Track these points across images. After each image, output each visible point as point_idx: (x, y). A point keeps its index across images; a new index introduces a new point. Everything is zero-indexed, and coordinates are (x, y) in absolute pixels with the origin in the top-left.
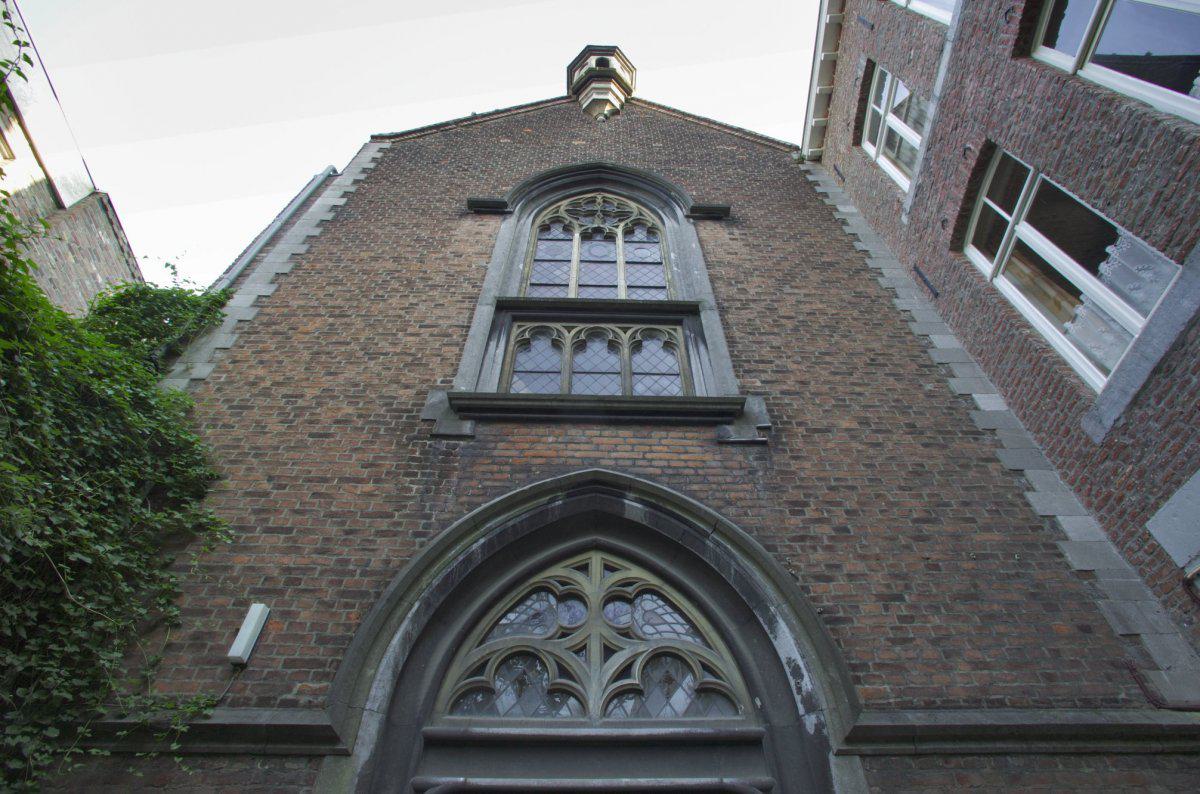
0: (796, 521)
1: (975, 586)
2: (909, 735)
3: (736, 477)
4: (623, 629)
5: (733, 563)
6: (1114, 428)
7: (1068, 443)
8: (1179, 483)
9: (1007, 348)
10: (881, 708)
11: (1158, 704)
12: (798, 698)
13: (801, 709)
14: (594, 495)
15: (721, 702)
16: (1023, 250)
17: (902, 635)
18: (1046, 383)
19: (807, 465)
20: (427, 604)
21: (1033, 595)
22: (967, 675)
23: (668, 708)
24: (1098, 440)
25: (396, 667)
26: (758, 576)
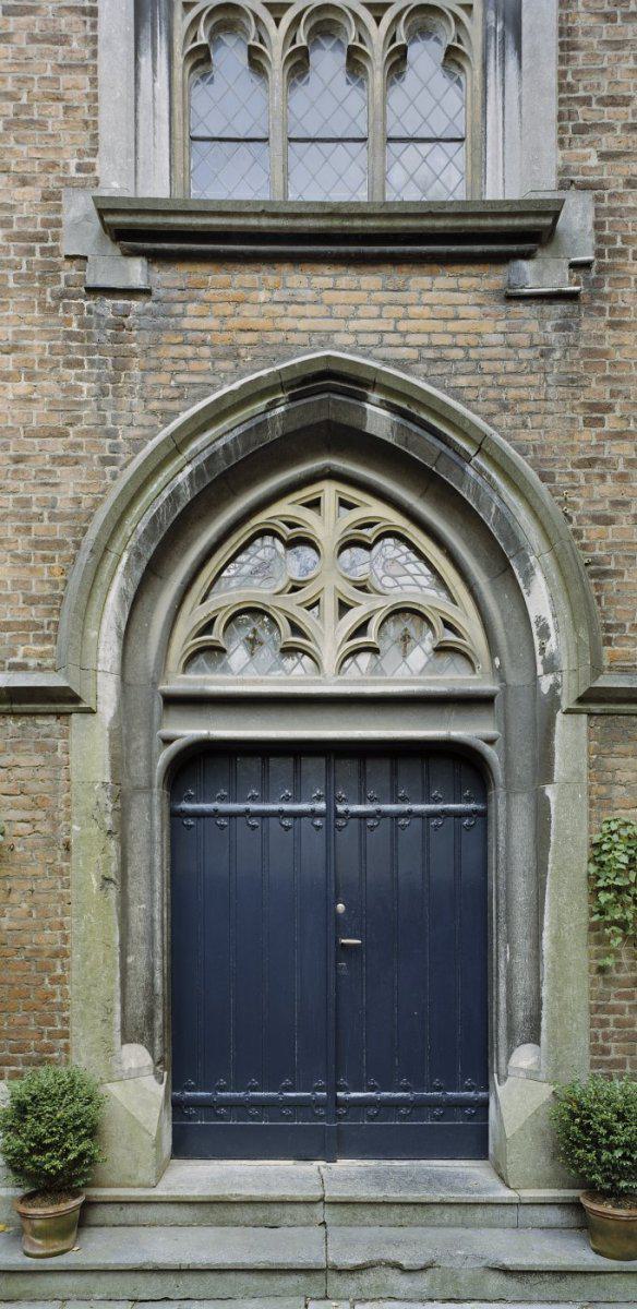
0: (591, 435)
5: (496, 498)
12: (539, 659)
13: (540, 670)
15: (459, 662)
26: (523, 517)
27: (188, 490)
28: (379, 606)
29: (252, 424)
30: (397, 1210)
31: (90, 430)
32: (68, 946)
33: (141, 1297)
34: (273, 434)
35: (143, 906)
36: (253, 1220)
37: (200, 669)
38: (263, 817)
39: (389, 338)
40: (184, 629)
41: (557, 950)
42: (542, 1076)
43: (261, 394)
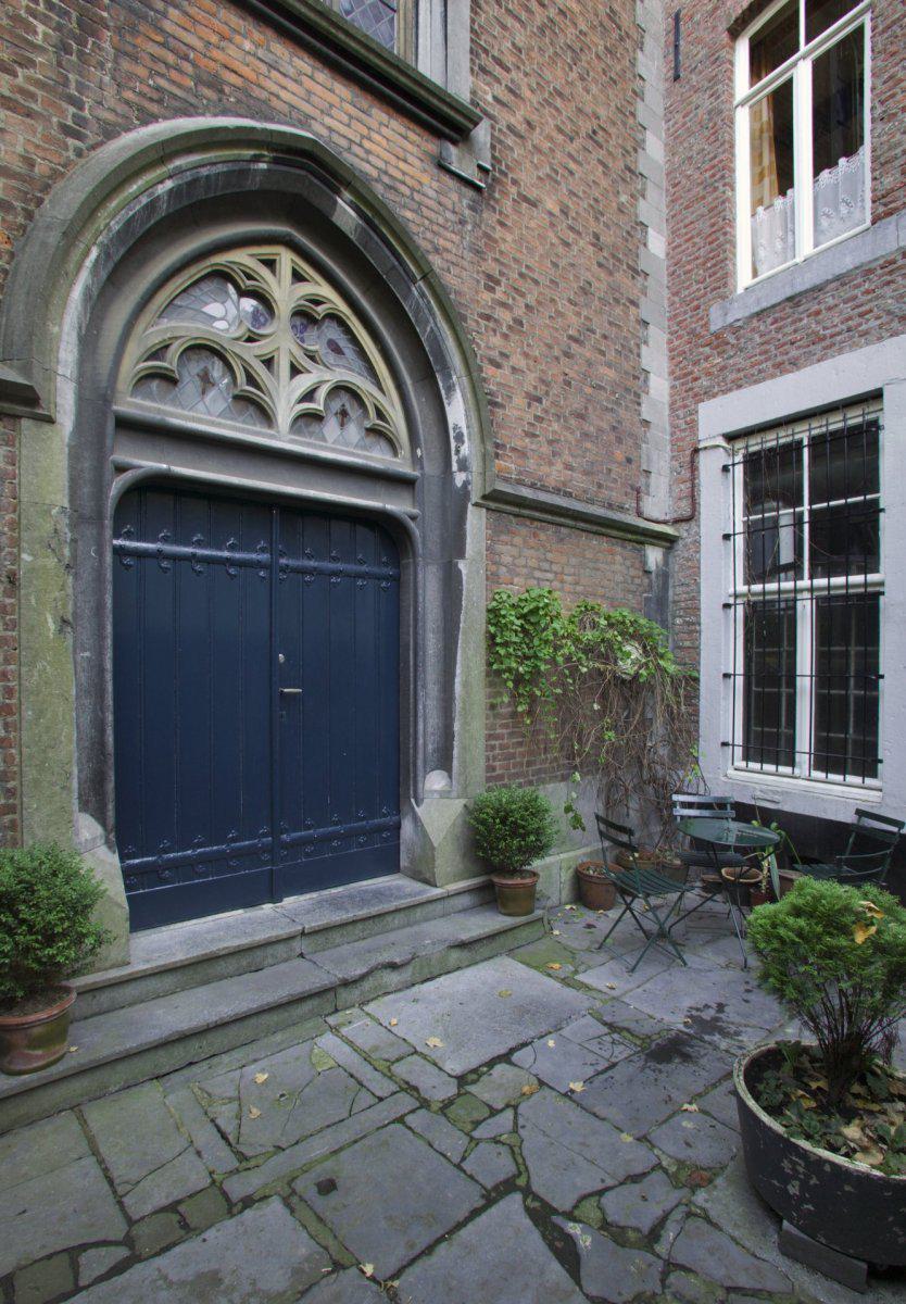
0: (486, 296)
1: (586, 408)
2: (520, 502)
3: (447, 220)
4: (311, 351)
5: (432, 321)
6: (731, 325)
7: (691, 317)
8: (740, 387)
9: (703, 198)
10: (506, 480)
11: (639, 514)
12: (454, 458)
13: (455, 467)
14: (303, 173)
15: (383, 444)
16: (782, 100)
17: (531, 430)
18: (711, 255)
19: (509, 238)
20: (106, 254)
21: (614, 428)
22: (559, 472)
23: (201, 403)
24: (713, 328)
25: (80, 328)
26: (450, 344)
27: (165, 205)
28: (327, 379)
29: (236, 167)
30: (360, 926)
31: (48, 85)
32: (13, 701)
33: (164, 1071)
34: (252, 184)
35: (87, 654)
36: (238, 969)
37: (150, 396)
38: (240, 567)
39: (356, 149)
40: (134, 351)
41: (467, 693)
42: (454, 794)
43: (249, 144)
